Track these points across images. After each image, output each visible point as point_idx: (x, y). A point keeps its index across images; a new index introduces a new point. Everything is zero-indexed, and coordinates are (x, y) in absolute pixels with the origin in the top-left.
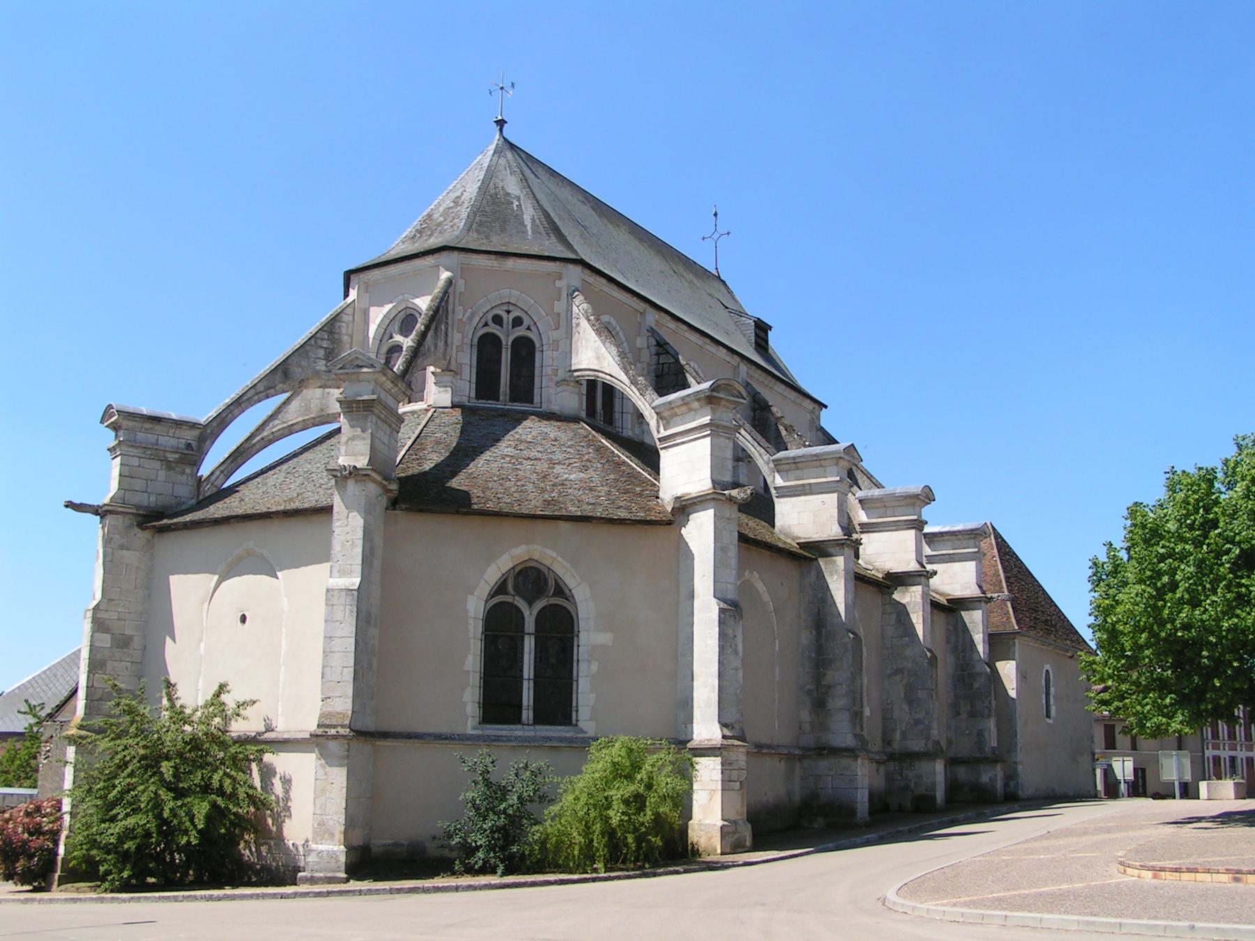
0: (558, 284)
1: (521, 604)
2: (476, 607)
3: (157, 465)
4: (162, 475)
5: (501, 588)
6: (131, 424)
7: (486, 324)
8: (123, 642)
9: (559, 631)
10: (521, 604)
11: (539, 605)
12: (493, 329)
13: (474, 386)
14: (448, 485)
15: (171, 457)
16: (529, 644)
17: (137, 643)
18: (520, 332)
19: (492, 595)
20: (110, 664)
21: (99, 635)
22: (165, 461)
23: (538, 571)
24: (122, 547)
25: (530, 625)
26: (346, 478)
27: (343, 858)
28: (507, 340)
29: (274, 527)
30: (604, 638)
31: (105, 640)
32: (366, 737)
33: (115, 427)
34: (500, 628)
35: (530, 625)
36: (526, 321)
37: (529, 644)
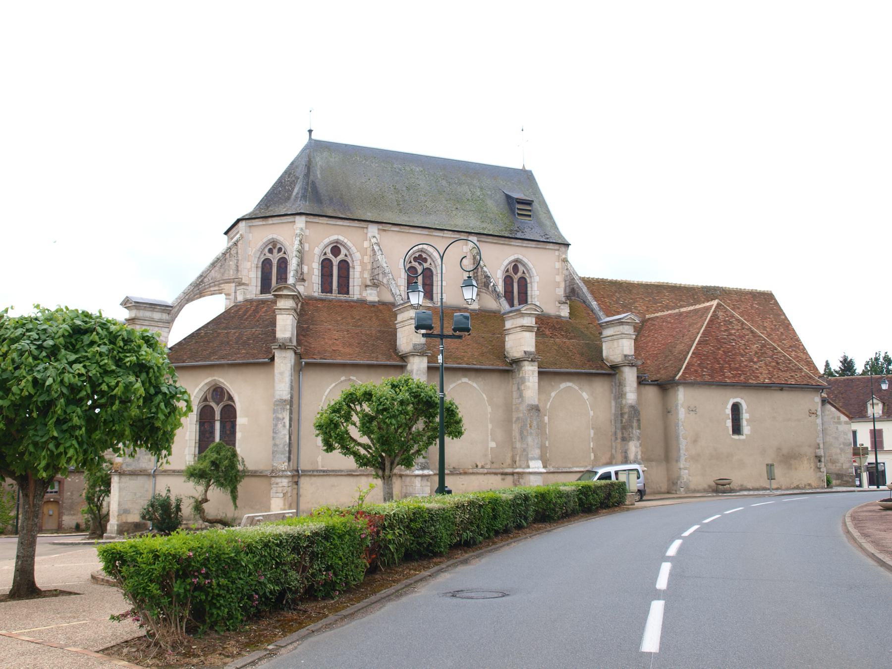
1: (213, 404)
9: (229, 414)
10: (213, 404)
11: (221, 405)
16: (218, 425)
25: (218, 416)
28: (335, 261)
35: (218, 416)
37: (218, 425)
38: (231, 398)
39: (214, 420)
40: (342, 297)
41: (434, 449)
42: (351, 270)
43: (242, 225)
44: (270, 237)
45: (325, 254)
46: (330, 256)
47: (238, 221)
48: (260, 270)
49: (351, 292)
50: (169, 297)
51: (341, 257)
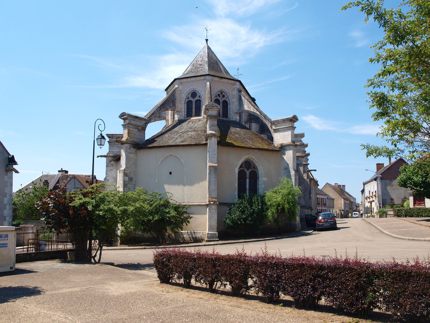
0: (234, 87)
1: (246, 170)
2: (237, 170)
3: (136, 130)
4: (138, 133)
5: (241, 166)
6: (130, 118)
7: (216, 96)
8: (131, 179)
9: (254, 176)
10: (246, 170)
11: (250, 171)
12: (218, 98)
13: (186, 113)
14: (146, 139)
15: (140, 128)
16: (248, 180)
17: (134, 179)
18: (224, 99)
19: (239, 168)
20: (128, 185)
21: (126, 177)
22: (138, 129)
23: (249, 162)
24: (130, 153)
25: (248, 176)
26: (212, 136)
27: (217, 235)
28: (194, 100)
29: (180, 149)
30: (265, 179)
31: (127, 179)
32: (221, 205)
33: (124, 119)
34: (241, 175)
35: (248, 176)
36: (226, 96)
37: (248, 180)
38: (255, 167)
39: (246, 178)
40: (225, 119)
41: (391, 210)
42: (229, 105)
43: (177, 81)
44: (221, 88)
45: (188, 98)
46: (191, 99)
47: (175, 80)
48: (186, 105)
49: (229, 117)
50: (143, 114)
51: (197, 98)
